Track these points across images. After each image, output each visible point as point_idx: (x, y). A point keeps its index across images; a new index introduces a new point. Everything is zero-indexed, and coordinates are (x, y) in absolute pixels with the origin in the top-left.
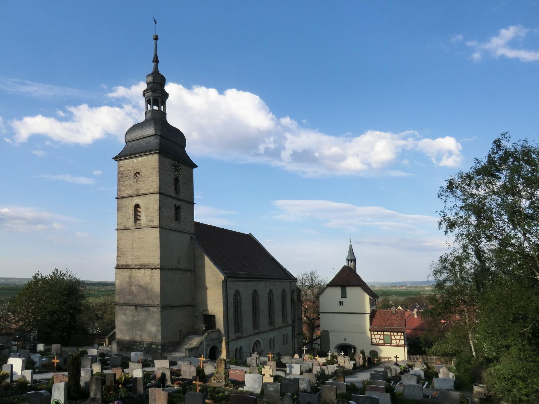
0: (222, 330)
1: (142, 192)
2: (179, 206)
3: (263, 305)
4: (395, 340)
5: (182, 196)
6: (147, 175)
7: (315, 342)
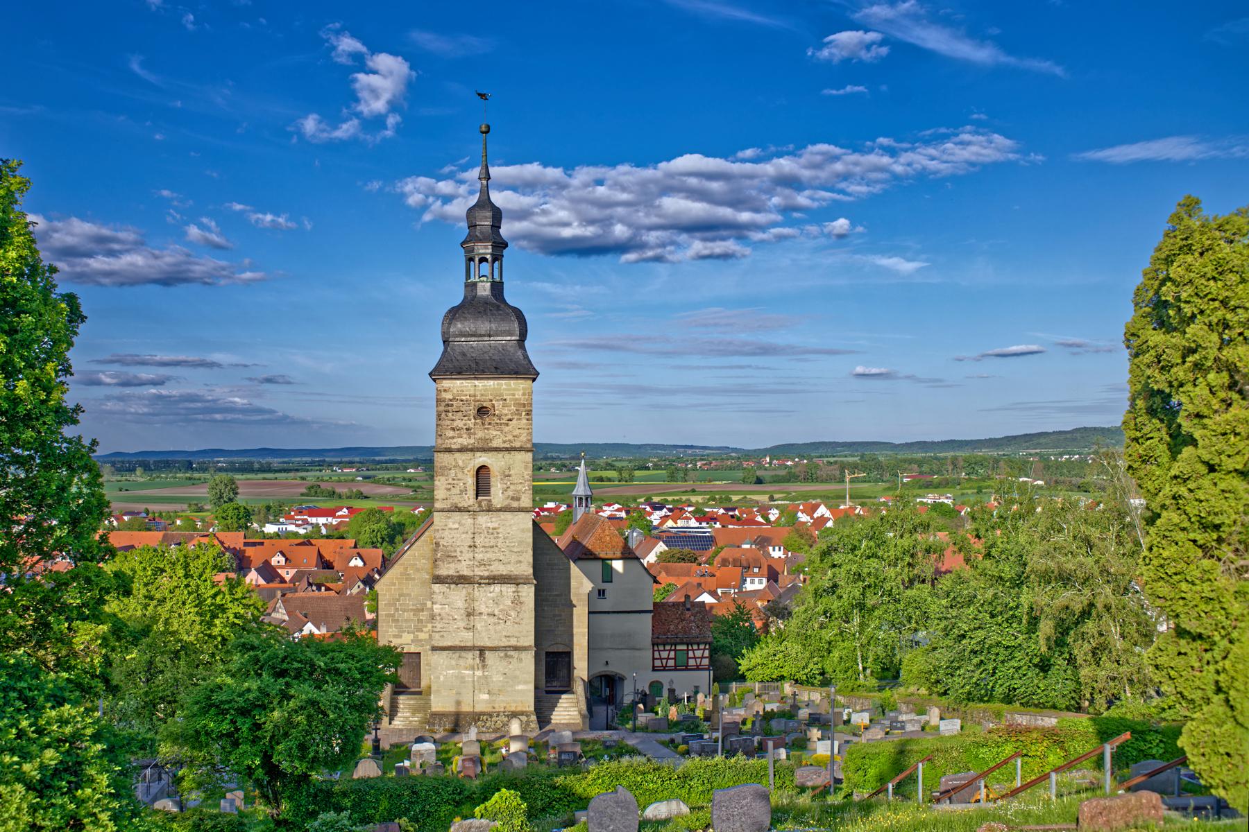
1: (495, 444)
4: (695, 658)
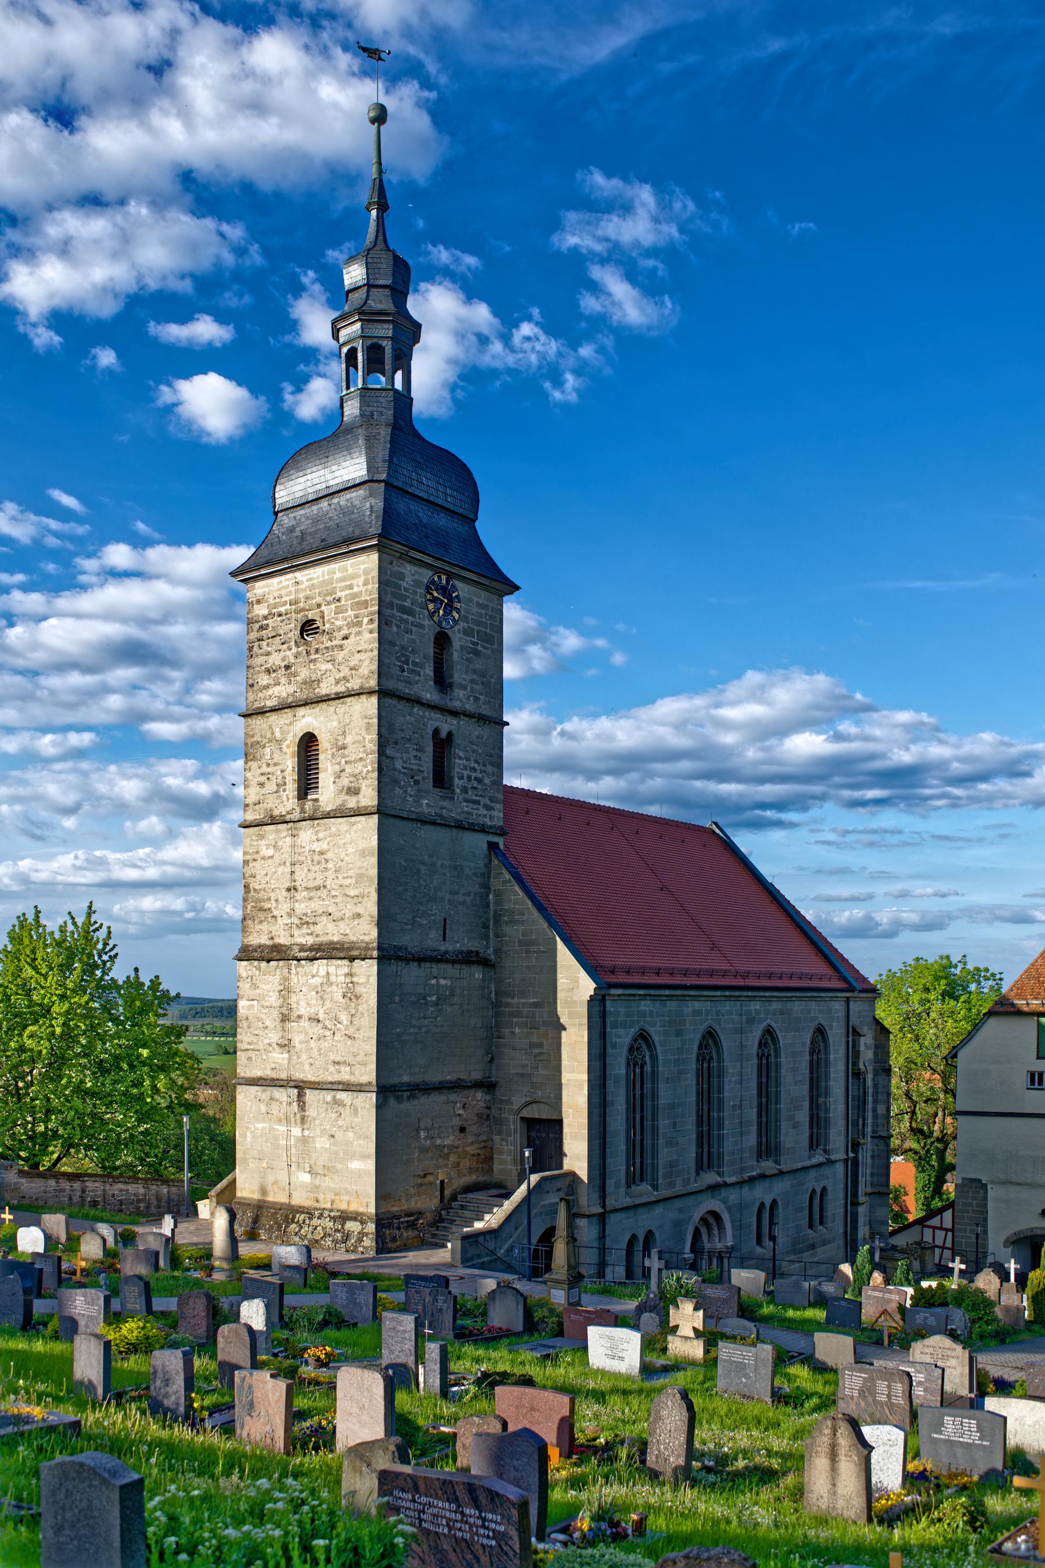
0: (583, 1174)
1: (326, 688)
2: (450, 734)
3: (738, 1081)
5: (459, 698)
6: (340, 629)
7: (935, 1221)
